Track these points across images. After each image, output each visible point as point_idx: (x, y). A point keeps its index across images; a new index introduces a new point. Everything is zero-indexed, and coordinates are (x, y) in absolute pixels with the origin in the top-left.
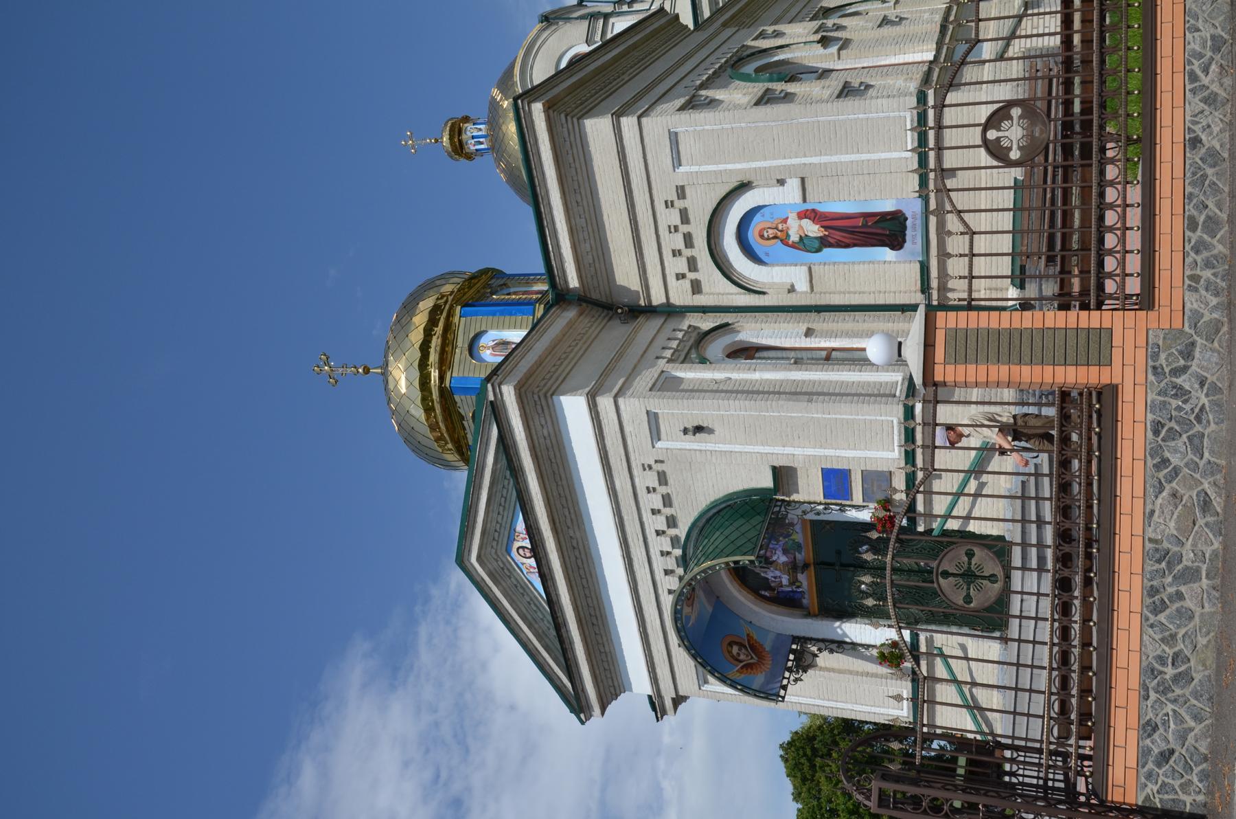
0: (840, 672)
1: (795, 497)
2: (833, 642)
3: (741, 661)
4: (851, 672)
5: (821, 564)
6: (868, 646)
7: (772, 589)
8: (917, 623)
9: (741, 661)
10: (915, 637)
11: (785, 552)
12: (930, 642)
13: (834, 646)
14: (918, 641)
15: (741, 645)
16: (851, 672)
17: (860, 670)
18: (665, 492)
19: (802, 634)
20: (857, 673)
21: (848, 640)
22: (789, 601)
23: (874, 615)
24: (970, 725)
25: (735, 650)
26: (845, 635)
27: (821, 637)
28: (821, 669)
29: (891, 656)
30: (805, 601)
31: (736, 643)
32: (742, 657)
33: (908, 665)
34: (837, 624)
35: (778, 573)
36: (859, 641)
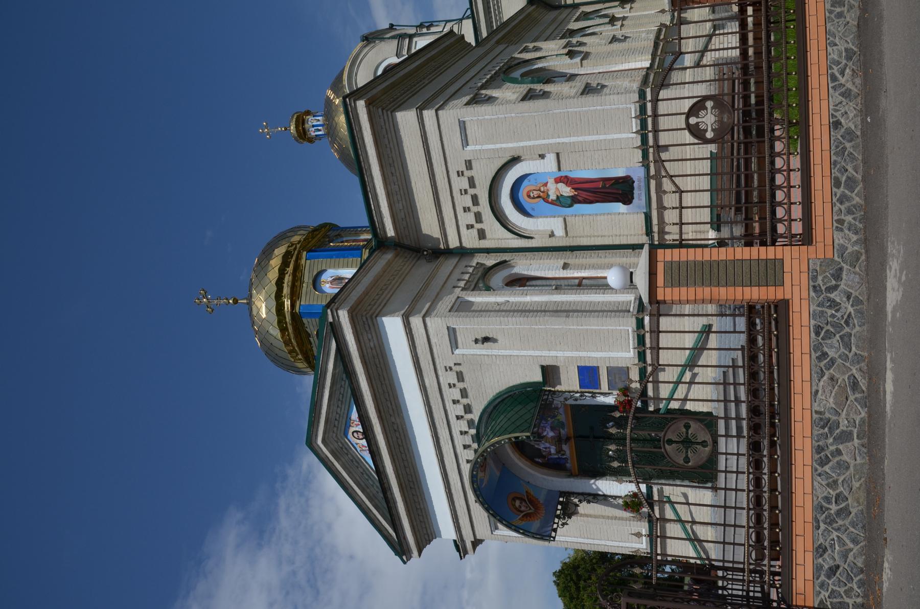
0: (596, 517)
1: (558, 388)
2: (589, 494)
3: (522, 512)
4: (603, 517)
5: (579, 437)
6: (615, 497)
7: (544, 457)
8: (651, 478)
9: (522, 512)
10: (650, 489)
11: (552, 429)
12: (661, 492)
13: (590, 498)
14: (652, 492)
15: (522, 500)
16: (603, 517)
17: (610, 515)
18: (462, 387)
19: (567, 490)
20: (608, 517)
21: (600, 493)
22: (556, 466)
23: (619, 474)
24: (692, 554)
25: (517, 503)
26: (598, 489)
27: (581, 491)
28: (582, 515)
29: (632, 504)
30: (568, 465)
31: (518, 498)
32: (523, 508)
33: (645, 510)
34: (592, 481)
35: (547, 445)
36: (608, 493)
